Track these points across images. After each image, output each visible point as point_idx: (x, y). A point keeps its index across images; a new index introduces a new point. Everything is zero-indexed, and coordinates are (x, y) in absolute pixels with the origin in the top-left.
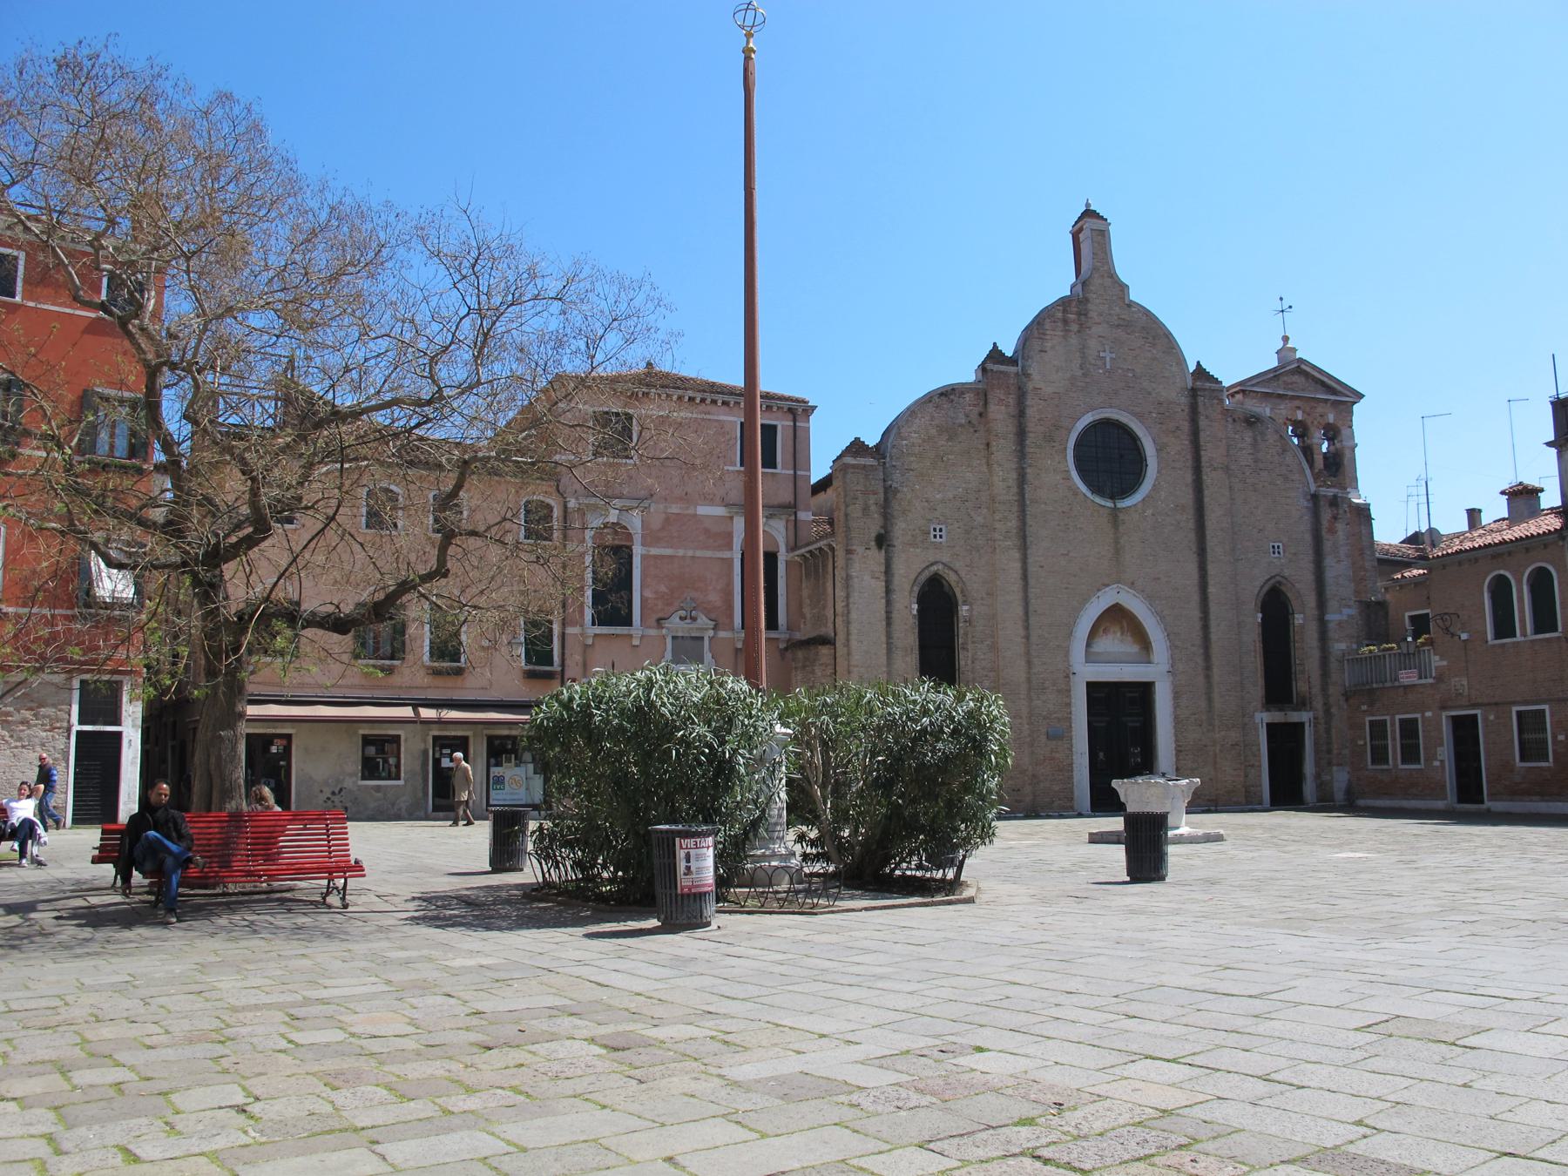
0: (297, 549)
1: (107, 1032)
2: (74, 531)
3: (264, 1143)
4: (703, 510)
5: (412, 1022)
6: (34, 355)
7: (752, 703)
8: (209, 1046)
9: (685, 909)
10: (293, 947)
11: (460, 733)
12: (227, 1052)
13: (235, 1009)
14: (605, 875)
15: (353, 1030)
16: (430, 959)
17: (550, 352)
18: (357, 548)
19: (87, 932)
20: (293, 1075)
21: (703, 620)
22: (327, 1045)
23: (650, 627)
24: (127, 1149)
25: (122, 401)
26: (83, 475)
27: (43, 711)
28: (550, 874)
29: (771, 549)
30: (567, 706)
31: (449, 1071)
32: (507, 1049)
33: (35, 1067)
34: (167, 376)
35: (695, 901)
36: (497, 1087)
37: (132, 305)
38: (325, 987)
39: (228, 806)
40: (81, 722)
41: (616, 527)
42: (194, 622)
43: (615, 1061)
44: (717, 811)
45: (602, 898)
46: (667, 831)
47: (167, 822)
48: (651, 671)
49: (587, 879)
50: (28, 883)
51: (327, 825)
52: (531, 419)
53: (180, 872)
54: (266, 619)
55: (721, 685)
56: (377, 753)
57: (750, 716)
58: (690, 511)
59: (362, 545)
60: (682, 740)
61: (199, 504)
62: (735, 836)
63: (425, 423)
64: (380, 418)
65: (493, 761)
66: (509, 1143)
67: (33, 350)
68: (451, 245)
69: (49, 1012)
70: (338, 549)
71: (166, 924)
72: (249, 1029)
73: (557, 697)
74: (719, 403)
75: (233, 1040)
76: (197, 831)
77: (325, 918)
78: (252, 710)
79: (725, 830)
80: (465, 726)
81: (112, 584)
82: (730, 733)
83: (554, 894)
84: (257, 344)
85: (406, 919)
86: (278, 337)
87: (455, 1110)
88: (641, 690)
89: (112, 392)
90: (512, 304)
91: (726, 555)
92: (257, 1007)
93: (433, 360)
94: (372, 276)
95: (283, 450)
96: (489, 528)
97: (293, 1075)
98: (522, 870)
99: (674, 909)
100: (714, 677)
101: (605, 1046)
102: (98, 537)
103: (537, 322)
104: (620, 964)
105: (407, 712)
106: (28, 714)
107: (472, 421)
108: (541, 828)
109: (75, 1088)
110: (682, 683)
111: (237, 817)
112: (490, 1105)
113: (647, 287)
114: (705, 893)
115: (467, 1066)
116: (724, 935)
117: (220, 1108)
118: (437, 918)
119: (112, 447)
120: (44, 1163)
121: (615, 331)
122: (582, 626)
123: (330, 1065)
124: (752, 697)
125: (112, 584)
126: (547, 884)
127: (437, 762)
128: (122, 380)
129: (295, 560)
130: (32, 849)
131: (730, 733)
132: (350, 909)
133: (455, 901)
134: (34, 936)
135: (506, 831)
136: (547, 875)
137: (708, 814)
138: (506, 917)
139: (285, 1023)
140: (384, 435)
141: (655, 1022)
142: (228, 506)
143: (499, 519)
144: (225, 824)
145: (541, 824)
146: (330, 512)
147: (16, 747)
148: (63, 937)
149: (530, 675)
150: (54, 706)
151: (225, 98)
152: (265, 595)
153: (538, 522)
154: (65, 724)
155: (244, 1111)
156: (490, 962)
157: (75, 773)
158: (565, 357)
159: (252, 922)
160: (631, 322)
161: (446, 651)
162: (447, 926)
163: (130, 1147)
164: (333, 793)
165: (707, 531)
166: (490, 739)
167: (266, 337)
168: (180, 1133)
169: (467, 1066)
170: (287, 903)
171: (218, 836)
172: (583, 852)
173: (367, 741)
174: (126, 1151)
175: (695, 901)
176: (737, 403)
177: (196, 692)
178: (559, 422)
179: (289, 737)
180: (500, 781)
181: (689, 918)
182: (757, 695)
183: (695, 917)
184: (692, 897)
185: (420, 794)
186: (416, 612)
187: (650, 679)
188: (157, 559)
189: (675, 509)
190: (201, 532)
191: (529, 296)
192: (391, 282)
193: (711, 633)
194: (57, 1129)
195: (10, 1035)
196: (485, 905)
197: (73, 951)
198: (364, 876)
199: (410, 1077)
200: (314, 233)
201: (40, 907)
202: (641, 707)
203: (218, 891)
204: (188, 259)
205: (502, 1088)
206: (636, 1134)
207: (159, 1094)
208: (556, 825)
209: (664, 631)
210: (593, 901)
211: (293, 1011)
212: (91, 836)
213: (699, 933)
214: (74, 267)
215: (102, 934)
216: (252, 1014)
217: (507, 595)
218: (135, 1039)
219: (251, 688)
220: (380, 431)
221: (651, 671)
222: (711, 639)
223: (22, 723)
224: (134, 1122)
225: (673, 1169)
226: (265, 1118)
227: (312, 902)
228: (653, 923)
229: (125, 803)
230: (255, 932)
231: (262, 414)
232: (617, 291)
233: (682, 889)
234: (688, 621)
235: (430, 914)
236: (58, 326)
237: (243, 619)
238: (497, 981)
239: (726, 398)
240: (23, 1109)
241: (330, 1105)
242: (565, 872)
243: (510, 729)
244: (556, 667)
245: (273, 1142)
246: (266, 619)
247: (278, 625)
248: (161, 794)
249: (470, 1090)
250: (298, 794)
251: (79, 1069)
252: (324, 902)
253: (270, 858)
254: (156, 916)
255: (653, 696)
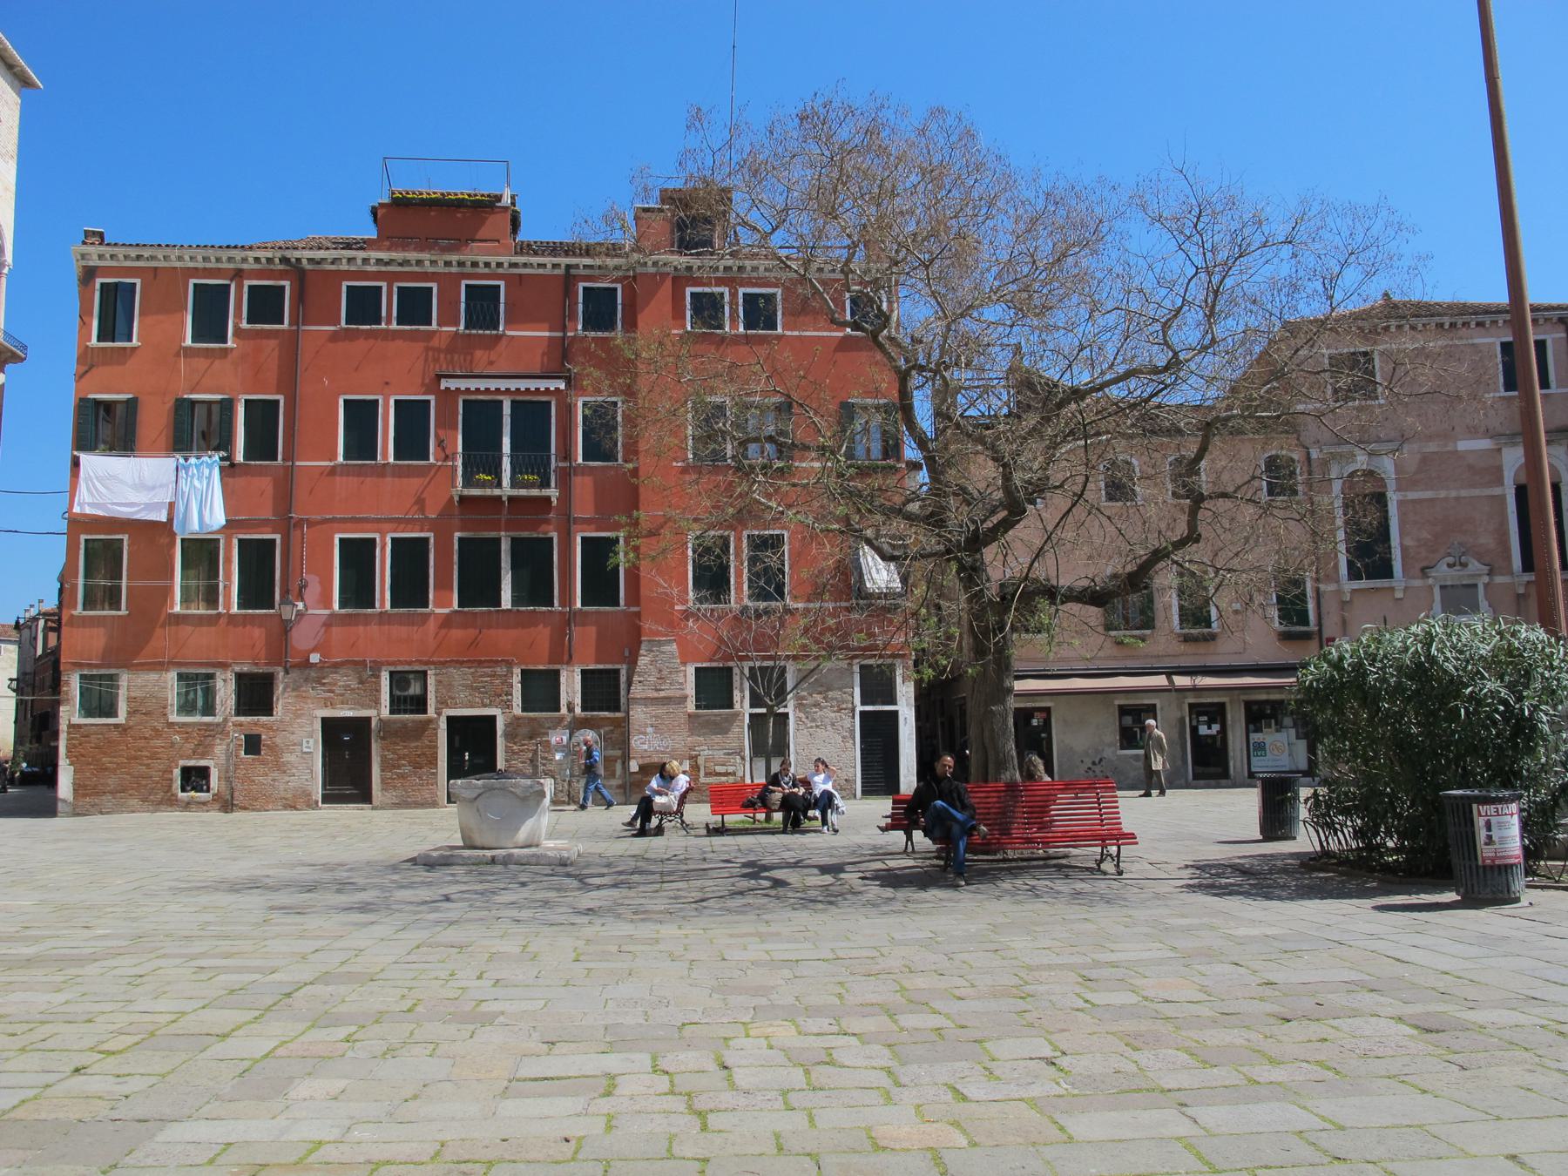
0: (1050, 528)
1: (920, 982)
2: (851, 530)
3: (1077, 1095)
4: (1463, 445)
5: (1203, 989)
6: (804, 377)
7: (1552, 653)
8: (1012, 1001)
9: (1489, 882)
10: (1076, 912)
11: (1216, 700)
12: (1029, 1007)
13: (1030, 969)
14: (1390, 844)
15: (1145, 993)
16: (1212, 928)
17: (1284, 300)
18: (1106, 522)
19: (889, 892)
20: (1094, 1033)
21: (1475, 566)
22: (1122, 1006)
23: (1414, 578)
24: (955, 1088)
25: (877, 408)
26: (851, 479)
27: (830, 694)
28: (1328, 843)
29: (1556, 480)
30: (1337, 665)
31: (1249, 1041)
32: (1308, 1022)
33: (867, 1009)
34: (916, 379)
35: (1500, 873)
36: (1302, 1061)
37: (880, 319)
38: (1112, 951)
39: (1003, 776)
40: (863, 703)
41: (1370, 474)
42: (958, 605)
43: (1430, 1043)
44: (1518, 775)
45: (1388, 869)
46: (1462, 797)
47: (951, 792)
48: (1428, 623)
49: (1370, 848)
50: (833, 848)
51: (1098, 794)
52: (1271, 369)
53: (965, 838)
54: (1028, 597)
55: (1514, 635)
56: (1134, 722)
57: (1552, 668)
58: (1450, 448)
59: (1109, 518)
60: (1472, 696)
61: (955, 494)
62: (1542, 802)
63: (1163, 389)
64: (1115, 392)
65: (1251, 727)
66: (1324, 1119)
67: (802, 373)
68: (1171, 208)
69: (869, 961)
70: (1086, 525)
71: (956, 887)
72: (1047, 987)
73: (1325, 657)
74: (1473, 325)
75: (1032, 996)
76: (977, 800)
77: (1103, 884)
78: (1019, 686)
79: (1529, 795)
80: (1221, 693)
81: (880, 575)
82: (1528, 688)
83: (1333, 864)
84: (994, 336)
85: (1182, 887)
86: (1011, 326)
87: (1261, 1080)
88: (1419, 646)
89: (869, 401)
90: (1240, 257)
91: (1497, 491)
92: (1050, 967)
93: (1166, 326)
94: (1094, 252)
95: (1030, 433)
96: (1238, 488)
97: (1094, 1033)
98: (1295, 838)
99: (1475, 882)
100: (1503, 627)
101: (1416, 1027)
102: (869, 533)
103: (1267, 270)
104: (1418, 939)
105: (1161, 681)
106: (818, 697)
107: (1210, 381)
108: (1315, 795)
109: (902, 1029)
110: (1466, 635)
111: (1012, 787)
112: (1296, 1078)
113: (1384, 213)
114: (1512, 866)
115: (1266, 1037)
116: (1539, 913)
117: (1031, 1059)
118: (1212, 886)
119: (868, 450)
120: (888, 1093)
121: (1352, 266)
122: (1337, 581)
123: (1128, 1026)
124: (1550, 645)
125: (880, 575)
126: (1326, 853)
127: (1194, 730)
128: (876, 388)
129: (1049, 538)
130: (832, 817)
131: (1528, 688)
132: (1124, 876)
133: (1229, 870)
134: (847, 894)
135: (1278, 798)
136: (1325, 844)
137: (1507, 778)
138: (1284, 887)
139: (1078, 983)
140: (1120, 409)
141: (1471, 1004)
142: (981, 493)
143: (1247, 478)
144: (1003, 794)
145: (1316, 791)
146: (1078, 489)
147: (811, 727)
148: (870, 896)
149: (1286, 637)
150: (840, 689)
151: (937, 112)
152: (1024, 574)
153: (1279, 476)
154: (850, 706)
155: (1054, 1064)
156: (1275, 932)
157: (861, 750)
158: (1301, 302)
159: (1034, 887)
160: (1371, 253)
161: (1195, 616)
162: (1225, 894)
163: (958, 1086)
164: (1094, 763)
165: (1470, 467)
166: (1248, 705)
167: (1000, 329)
168: (998, 1078)
169: (1266, 1037)
170: (1064, 869)
171: (997, 805)
172: (1362, 819)
173: (1124, 711)
174: (955, 1090)
175: (1500, 873)
176: (1494, 322)
177: (970, 671)
178: (1302, 370)
179: (1048, 710)
180: (1261, 747)
181: (1494, 893)
182: (1558, 644)
183: (1502, 892)
184: (1496, 869)
185: (1179, 763)
186: (1166, 580)
187: (1429, 633)
188: (924, 549)
189: (1432, 447)
190: (958, 517)
191: (1257, 244)
192: (1115, 255)
193: (1486, 579)
194: (894, 1064)
195: (840, 979)
196: (1261, 874)
197: (880, 909)
198: (1137, 843)
199: (1209, 1043)
200: (1034, 221)
201: (848, 868)
202: (1422, 664)
203: (999, 856)
204: (927, 267)
205: (1307, 1062)
206: (1467, 1124)
207: (975, 1041)
208: (1332, 791)
209: (1430, 581)
210: (1379, 871)
211: (1084, 972)
212: (883, 806)
213: (1507, 909)
214: (828, 294)
215: (902, 894)
216: (1047, 973)
217: (1264, 556)
218: (946, 990)
219: (1017, 665)
220: (1116, 404)
221: (1428, 623)
222: (1486, 586)
223: (815, 706)
224: (958, 1064)
225: (1519, 1169)
226: (1074, 1071)
227: (1087, 869)
228: (1451, 896)
229: (905, 777)
230: (1037, 896)
231: (999, 402)
232: (1351, 223)
233: (1484, 861)
234: (1458, 568)
235: (1205, 882)
236: (820, 348)
237: (1005, 599)
238: (1286, 952)
239: (1480, 318)
240: (863, 1043)
241: (1134, 1065)
242: (1343, 840)
243: (1268, 693)
244: (1313, 627)
245: (1085, 1095)
246: (1028, 597)
247: (1043, 603)
248: (945, 765)
249: (1274, 1061)
250: (1059, 766)
251: (903, 1013)
252: (1099, 869)
253: (1043, 827)
254: (946, 879)
255: (1434, 651)
